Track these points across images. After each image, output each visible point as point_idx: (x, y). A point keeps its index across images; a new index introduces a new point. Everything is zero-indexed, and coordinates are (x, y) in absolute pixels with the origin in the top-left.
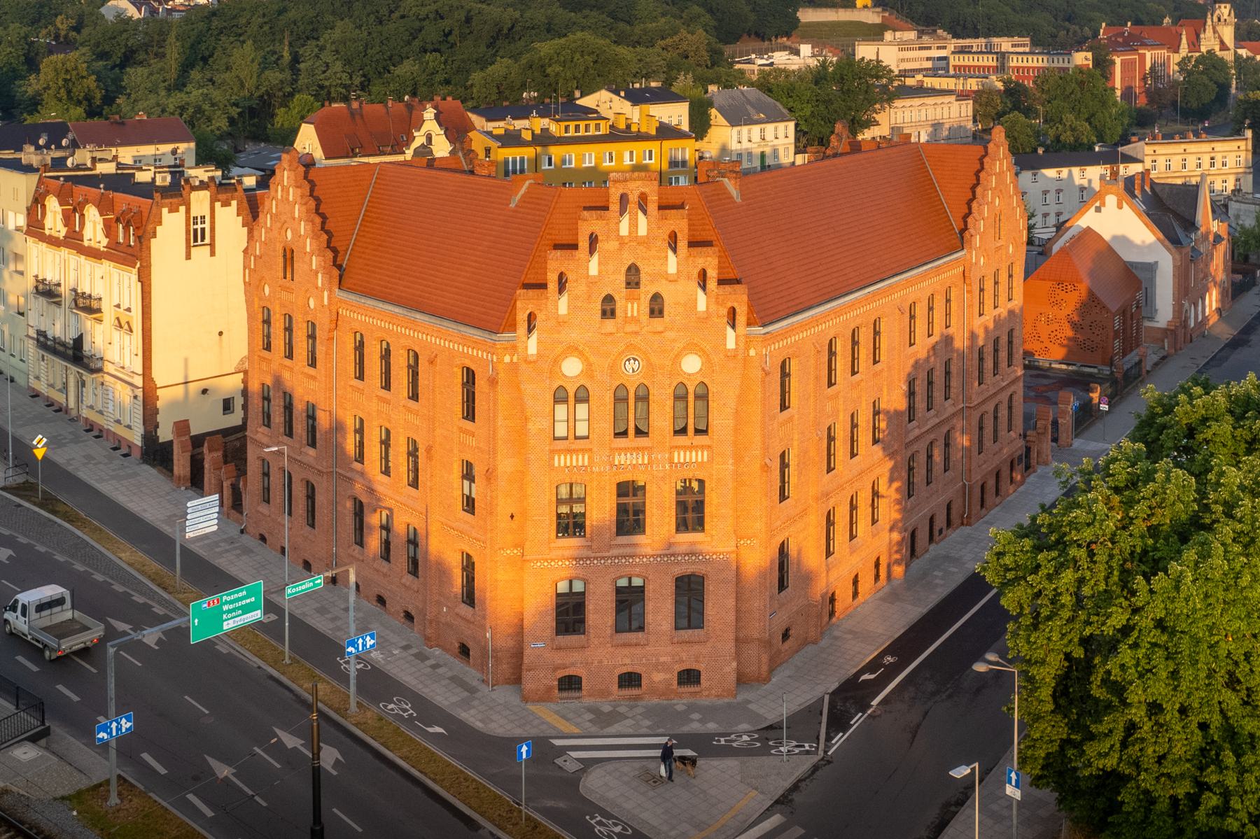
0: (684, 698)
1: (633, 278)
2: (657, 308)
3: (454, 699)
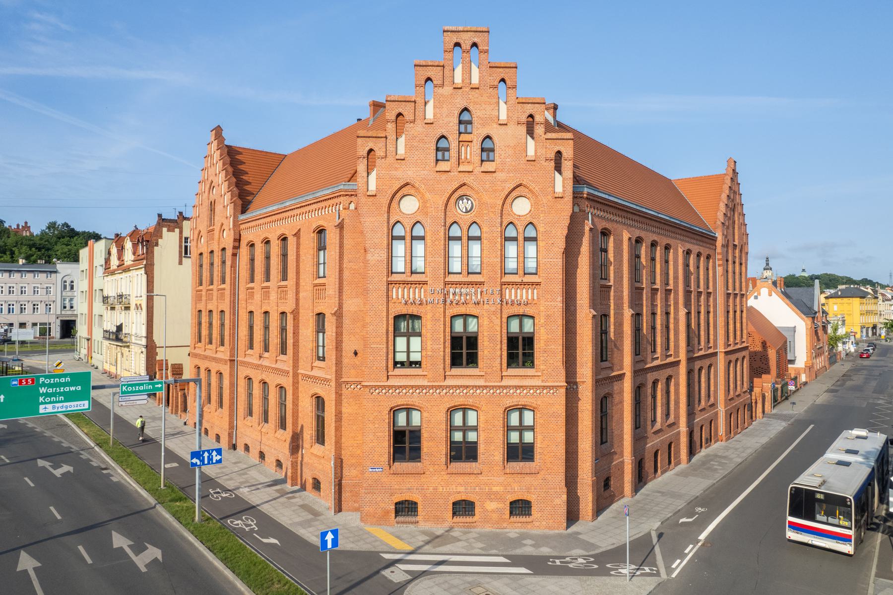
0: (515, 527)
1: (464, 120)
2: (487, 151)
3: (298, 520)
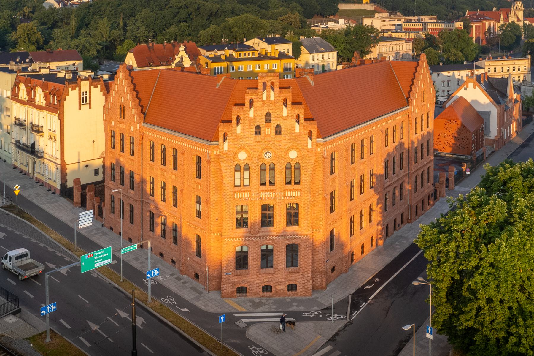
0: (290, 296)
1: (268, 118)
2: (278, 131)
3: (193, 297)
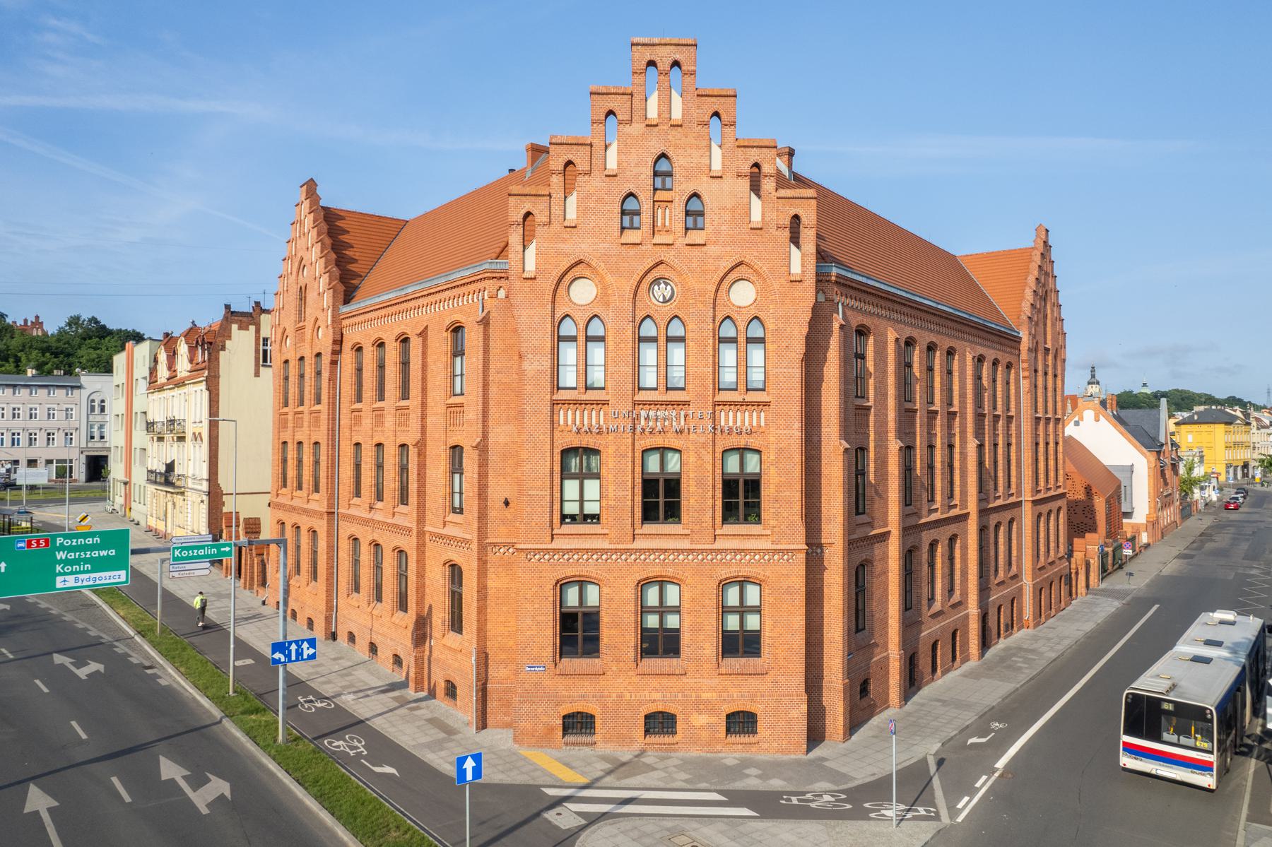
0: (733, 751)
1: (662, 171)
2: (694, 214)
3: (424, 740)
